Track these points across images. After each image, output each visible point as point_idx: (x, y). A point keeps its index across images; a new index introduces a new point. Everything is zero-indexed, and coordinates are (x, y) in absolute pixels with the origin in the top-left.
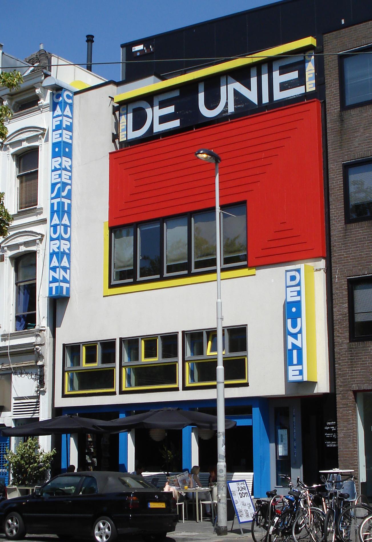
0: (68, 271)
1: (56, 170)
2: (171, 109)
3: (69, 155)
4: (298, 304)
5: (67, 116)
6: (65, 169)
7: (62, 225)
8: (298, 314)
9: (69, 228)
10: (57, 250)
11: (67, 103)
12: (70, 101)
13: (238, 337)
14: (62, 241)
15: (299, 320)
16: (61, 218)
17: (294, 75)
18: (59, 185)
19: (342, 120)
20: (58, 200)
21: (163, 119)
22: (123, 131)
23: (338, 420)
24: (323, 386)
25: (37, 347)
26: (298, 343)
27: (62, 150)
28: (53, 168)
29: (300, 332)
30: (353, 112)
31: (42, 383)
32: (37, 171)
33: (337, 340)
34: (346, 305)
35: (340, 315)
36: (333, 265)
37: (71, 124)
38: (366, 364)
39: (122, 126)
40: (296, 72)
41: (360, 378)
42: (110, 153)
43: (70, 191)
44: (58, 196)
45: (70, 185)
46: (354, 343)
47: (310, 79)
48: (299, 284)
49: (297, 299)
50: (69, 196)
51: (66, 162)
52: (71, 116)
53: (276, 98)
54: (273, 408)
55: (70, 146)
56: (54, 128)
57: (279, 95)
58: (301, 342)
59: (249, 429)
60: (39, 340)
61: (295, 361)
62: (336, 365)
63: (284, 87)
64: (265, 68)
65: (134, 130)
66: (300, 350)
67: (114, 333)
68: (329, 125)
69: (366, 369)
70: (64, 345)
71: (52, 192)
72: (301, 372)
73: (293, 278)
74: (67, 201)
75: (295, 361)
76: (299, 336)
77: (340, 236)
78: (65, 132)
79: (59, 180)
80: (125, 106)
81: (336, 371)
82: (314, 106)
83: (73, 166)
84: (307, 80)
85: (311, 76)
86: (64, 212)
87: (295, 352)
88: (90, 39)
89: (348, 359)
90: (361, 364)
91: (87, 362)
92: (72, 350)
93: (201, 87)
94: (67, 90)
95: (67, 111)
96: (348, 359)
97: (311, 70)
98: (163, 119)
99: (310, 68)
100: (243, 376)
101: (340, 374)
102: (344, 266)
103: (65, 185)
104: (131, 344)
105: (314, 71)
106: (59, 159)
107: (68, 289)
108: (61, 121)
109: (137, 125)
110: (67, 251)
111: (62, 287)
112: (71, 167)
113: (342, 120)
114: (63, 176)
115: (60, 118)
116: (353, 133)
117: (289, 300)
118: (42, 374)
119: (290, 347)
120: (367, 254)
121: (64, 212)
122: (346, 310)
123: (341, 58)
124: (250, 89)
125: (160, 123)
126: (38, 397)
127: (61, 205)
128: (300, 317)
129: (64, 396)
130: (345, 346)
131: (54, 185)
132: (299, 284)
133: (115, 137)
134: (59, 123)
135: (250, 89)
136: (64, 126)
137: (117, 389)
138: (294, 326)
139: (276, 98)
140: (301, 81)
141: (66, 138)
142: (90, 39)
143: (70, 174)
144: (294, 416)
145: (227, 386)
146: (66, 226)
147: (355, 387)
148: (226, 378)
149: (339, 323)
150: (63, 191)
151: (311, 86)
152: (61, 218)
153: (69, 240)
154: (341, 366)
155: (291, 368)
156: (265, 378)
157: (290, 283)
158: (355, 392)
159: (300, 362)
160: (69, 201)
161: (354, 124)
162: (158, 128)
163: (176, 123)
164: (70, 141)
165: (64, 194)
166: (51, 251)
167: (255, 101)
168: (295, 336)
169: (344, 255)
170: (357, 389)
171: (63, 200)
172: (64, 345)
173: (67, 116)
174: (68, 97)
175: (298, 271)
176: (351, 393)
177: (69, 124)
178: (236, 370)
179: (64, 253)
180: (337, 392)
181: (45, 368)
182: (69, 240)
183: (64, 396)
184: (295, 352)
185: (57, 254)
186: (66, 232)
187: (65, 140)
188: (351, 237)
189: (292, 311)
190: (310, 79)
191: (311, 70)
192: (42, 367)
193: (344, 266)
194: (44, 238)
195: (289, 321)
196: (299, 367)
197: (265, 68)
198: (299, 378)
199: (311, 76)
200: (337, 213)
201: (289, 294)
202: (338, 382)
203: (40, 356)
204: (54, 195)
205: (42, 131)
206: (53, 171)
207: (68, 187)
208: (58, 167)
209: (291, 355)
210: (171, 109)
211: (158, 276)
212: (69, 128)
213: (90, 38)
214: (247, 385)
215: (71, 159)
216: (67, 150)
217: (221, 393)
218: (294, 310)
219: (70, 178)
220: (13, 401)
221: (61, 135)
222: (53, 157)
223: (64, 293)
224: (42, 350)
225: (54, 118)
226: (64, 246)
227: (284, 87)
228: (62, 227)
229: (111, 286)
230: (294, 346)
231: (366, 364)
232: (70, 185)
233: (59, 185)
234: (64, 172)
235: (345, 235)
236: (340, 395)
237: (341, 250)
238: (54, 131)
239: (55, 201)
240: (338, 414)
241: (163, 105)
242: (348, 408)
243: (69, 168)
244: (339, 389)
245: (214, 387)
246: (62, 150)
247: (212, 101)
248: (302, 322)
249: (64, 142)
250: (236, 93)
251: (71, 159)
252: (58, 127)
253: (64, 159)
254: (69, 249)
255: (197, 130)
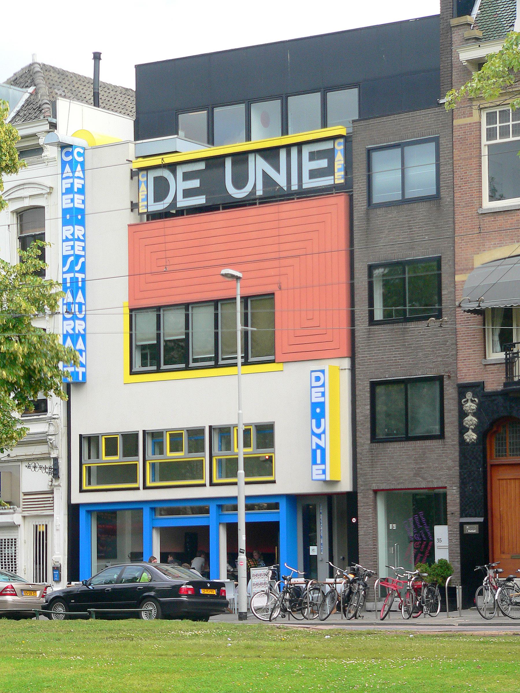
0: (84, 353)
1: (67, 240)
2: (195, 183)
3: (82, 223)
4: (322, 405)
5: (79, 178)
6: (79, 239)
7: (77, 303)
8: (322, 415)
9: (84, 307)
10: (71, 332)
11: (77, 162)
12: (80, 159)
13: (265, 434)
14: (77, 321)
15: (323, 420)
16: (74, 296)
17: (323, 163)
18: (72, 258)
19: (368, 220)
20: (72, 275)
21: (188, 193)
22: (143, 200)
23: (359, 518)
24: (346, 486)
25: (50, 437)
26: (321, 443)
27: (74, 217)
28: (64, 238)
29: (324, 432)
30: (380, 212)
31: (56, 474)
32: (44, 233)
33: (359, 440)
34: (368, 407)
35: (362, 416)
36: (357, 366)
37: (83, 186)
38: (385, 464)
39: (142, 196)
40: (326, 161)
41: (380, 478)
42: (129, 225)
43: (84, 263)
44: (71, 270)
45: (84, 256)
46: (374, 444)
47: (339, 170)
48: (323, 385)
49: (322, 400)
50: (83, 270)
51: (79, 231)
52: (82, 177)
53: (304, 186)
54: (304, 505)
55: (82, 212)
56: (64, 191)
57: (308, 183)
58: (326, 442)
59: (275, 526)
60: (52, 430)
61: (319, 461)
62: (358, 465)
63: (314, 174)
64: (294, 152)
65: (155, 201)
66: (323, 450)
67: (137, 425)
68: (356, 223)
69: (385, 470)
70: (81, 436)
71: (64, 265)
72: (324, 472)
73: (318, 379)
74: (80, 276)
75: (319, 461)
76: (323, 436)
77: (364, 338)
78: (77, 196)
79: (72, 252)
80: (145, 172)
81: (358, 470)
82: (339, 202)
83: (86, 235)
84: (336, 170)
85: (340, 166)
86: (78, 288)
87: (319, 452)
88: (97, 57)
89: (369, 460)
90: (381, 464)
91: (107, 454)
92: (90, 441)
93: (228, 163)
94: (77, 147)
95: (79, 173)
96: (369, 460)
97: (340, 160)
98: (188, 193)
99: (339, 160)
100: (271, 474)
101: (361, 474)
102: (367, 368)
103: (78, 257)
104: (156, 436)
105: (343, 162)
106: (71, 227)
107: (84, 374)
108: (72, 184)
109: (159, 196)
110: (82, 332)
111: (78, 373)
112: (84, 236)
113: (368, 219)
114: (77, 248)
115: (71, 180)
116: (378, 233)
117: (314, 400)
118: (55, 468)
119: (314, 447)
120: (388, 357)
121: (78, 288)
122: (368, 412)
123: (369, 152)
124: (278, 171)
125: (184, 180)
126: (52, 492)
127: (74, 281)
128: (324, 417)
129: (81, 491)
130: (367, 447)
131: (65, 258)
132: (323, 385)
133: (134, 206)
134: (69, 186)
135: (264, 172)
136: (76, 190)
137: (140, 483)
138: (318, 426)
139: (304, 186)
140: (330, 171)
141: (78, 204)
142: (97, 57)
143: (83, 244)
144: (320, 513)
145: (247, 483)
146: (80, 304)
147: (375, 487)
148: (246, 475)
149: (361, 424)
150: (77, 265)
151: (339, 178)
152: (74, 296)
153: (84, 319)
154: (363, 466)
155: (315, 467)
156: (293, 475)
157: (315, 384)
158: (376, 492)
159: (323, 462)
160: (83, 276)
161: (380, 225)
162: (183, 203)
163: (200, 200)
164: (82, 206)
165: (77, 268)
166: (65, 332)
167: (285, 189)
168: (319, 436)
169: (367, 357)
170: (377, 488)
171: (77, 275)
172: (81, 436)
173: (79, 178)
174: (79, 154)
175: (323, 371)
176: (372, 492)
177: (81, 186)
178: (261, 467)
179: (79, 334)
180: (358, 491)
181: (60, 461)
182: (84, 319)
183: (81, 491)
184: (319, 452)
185: (71, 336)
186: (80, 311)
187: (77, 205)
188: (374, 339)
189: (318, 412)
190: (339, 170)
191: (340, 160)
192: (56, 460)
193: (367, 368)
194: (54, 192)
195: (314, 421)
196: (323, 467)
197: (294, 152)
198: (323, 477)
199: (340, 166)
200: (362, 314)
201: (314, 395)
202: (360, 481)
203: (53, 447)
204: (66, 269)
205: (49, 191)
206: (63, 241)
207: (82, 260)
208: (70, 237)
209: (318, 455)
210: (195, 183)
211: (183, 366)
212: (82, 191)
213: (98, 55)
214: (274, 482)
215: (84, 226)
216: (79, 217)
217: (242, 489)
218: (318, 410)
219: (84, 249)
220: (22, 497)
221: (72, 200)
222: (64, 224)
223: (80, 378)
224: (57, 441)
225: (63, 179)
226: (80, 326)
227: (314, 174)
228: (77, 306)
229: (132, 373)
230: (318, 446)
231: (385, 464)
232: (84, 256)
233: (72, 258)
234: (77, 243)
235: (369, 337)
236: (362, 494)
237: (364, 351)
238: (63, 194)
239: (68, 276)
240: (359, 513)
241: (187, 176)
242: (368, 507)
243: (82, 238)
244: (360, 489)
245: (235, 484)
246: (74, 217)
247: (240, 181)
248: (326, 422)
249: (77, 208)
250: (265, 175)
251: (84, 226)
252: (69, 191)
253: (77, 227)
254: (84, 330)
255: (224, 211)
